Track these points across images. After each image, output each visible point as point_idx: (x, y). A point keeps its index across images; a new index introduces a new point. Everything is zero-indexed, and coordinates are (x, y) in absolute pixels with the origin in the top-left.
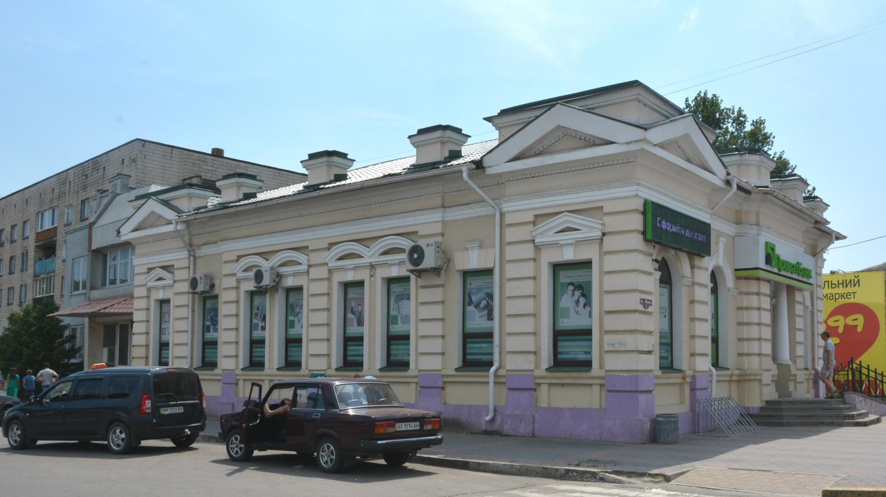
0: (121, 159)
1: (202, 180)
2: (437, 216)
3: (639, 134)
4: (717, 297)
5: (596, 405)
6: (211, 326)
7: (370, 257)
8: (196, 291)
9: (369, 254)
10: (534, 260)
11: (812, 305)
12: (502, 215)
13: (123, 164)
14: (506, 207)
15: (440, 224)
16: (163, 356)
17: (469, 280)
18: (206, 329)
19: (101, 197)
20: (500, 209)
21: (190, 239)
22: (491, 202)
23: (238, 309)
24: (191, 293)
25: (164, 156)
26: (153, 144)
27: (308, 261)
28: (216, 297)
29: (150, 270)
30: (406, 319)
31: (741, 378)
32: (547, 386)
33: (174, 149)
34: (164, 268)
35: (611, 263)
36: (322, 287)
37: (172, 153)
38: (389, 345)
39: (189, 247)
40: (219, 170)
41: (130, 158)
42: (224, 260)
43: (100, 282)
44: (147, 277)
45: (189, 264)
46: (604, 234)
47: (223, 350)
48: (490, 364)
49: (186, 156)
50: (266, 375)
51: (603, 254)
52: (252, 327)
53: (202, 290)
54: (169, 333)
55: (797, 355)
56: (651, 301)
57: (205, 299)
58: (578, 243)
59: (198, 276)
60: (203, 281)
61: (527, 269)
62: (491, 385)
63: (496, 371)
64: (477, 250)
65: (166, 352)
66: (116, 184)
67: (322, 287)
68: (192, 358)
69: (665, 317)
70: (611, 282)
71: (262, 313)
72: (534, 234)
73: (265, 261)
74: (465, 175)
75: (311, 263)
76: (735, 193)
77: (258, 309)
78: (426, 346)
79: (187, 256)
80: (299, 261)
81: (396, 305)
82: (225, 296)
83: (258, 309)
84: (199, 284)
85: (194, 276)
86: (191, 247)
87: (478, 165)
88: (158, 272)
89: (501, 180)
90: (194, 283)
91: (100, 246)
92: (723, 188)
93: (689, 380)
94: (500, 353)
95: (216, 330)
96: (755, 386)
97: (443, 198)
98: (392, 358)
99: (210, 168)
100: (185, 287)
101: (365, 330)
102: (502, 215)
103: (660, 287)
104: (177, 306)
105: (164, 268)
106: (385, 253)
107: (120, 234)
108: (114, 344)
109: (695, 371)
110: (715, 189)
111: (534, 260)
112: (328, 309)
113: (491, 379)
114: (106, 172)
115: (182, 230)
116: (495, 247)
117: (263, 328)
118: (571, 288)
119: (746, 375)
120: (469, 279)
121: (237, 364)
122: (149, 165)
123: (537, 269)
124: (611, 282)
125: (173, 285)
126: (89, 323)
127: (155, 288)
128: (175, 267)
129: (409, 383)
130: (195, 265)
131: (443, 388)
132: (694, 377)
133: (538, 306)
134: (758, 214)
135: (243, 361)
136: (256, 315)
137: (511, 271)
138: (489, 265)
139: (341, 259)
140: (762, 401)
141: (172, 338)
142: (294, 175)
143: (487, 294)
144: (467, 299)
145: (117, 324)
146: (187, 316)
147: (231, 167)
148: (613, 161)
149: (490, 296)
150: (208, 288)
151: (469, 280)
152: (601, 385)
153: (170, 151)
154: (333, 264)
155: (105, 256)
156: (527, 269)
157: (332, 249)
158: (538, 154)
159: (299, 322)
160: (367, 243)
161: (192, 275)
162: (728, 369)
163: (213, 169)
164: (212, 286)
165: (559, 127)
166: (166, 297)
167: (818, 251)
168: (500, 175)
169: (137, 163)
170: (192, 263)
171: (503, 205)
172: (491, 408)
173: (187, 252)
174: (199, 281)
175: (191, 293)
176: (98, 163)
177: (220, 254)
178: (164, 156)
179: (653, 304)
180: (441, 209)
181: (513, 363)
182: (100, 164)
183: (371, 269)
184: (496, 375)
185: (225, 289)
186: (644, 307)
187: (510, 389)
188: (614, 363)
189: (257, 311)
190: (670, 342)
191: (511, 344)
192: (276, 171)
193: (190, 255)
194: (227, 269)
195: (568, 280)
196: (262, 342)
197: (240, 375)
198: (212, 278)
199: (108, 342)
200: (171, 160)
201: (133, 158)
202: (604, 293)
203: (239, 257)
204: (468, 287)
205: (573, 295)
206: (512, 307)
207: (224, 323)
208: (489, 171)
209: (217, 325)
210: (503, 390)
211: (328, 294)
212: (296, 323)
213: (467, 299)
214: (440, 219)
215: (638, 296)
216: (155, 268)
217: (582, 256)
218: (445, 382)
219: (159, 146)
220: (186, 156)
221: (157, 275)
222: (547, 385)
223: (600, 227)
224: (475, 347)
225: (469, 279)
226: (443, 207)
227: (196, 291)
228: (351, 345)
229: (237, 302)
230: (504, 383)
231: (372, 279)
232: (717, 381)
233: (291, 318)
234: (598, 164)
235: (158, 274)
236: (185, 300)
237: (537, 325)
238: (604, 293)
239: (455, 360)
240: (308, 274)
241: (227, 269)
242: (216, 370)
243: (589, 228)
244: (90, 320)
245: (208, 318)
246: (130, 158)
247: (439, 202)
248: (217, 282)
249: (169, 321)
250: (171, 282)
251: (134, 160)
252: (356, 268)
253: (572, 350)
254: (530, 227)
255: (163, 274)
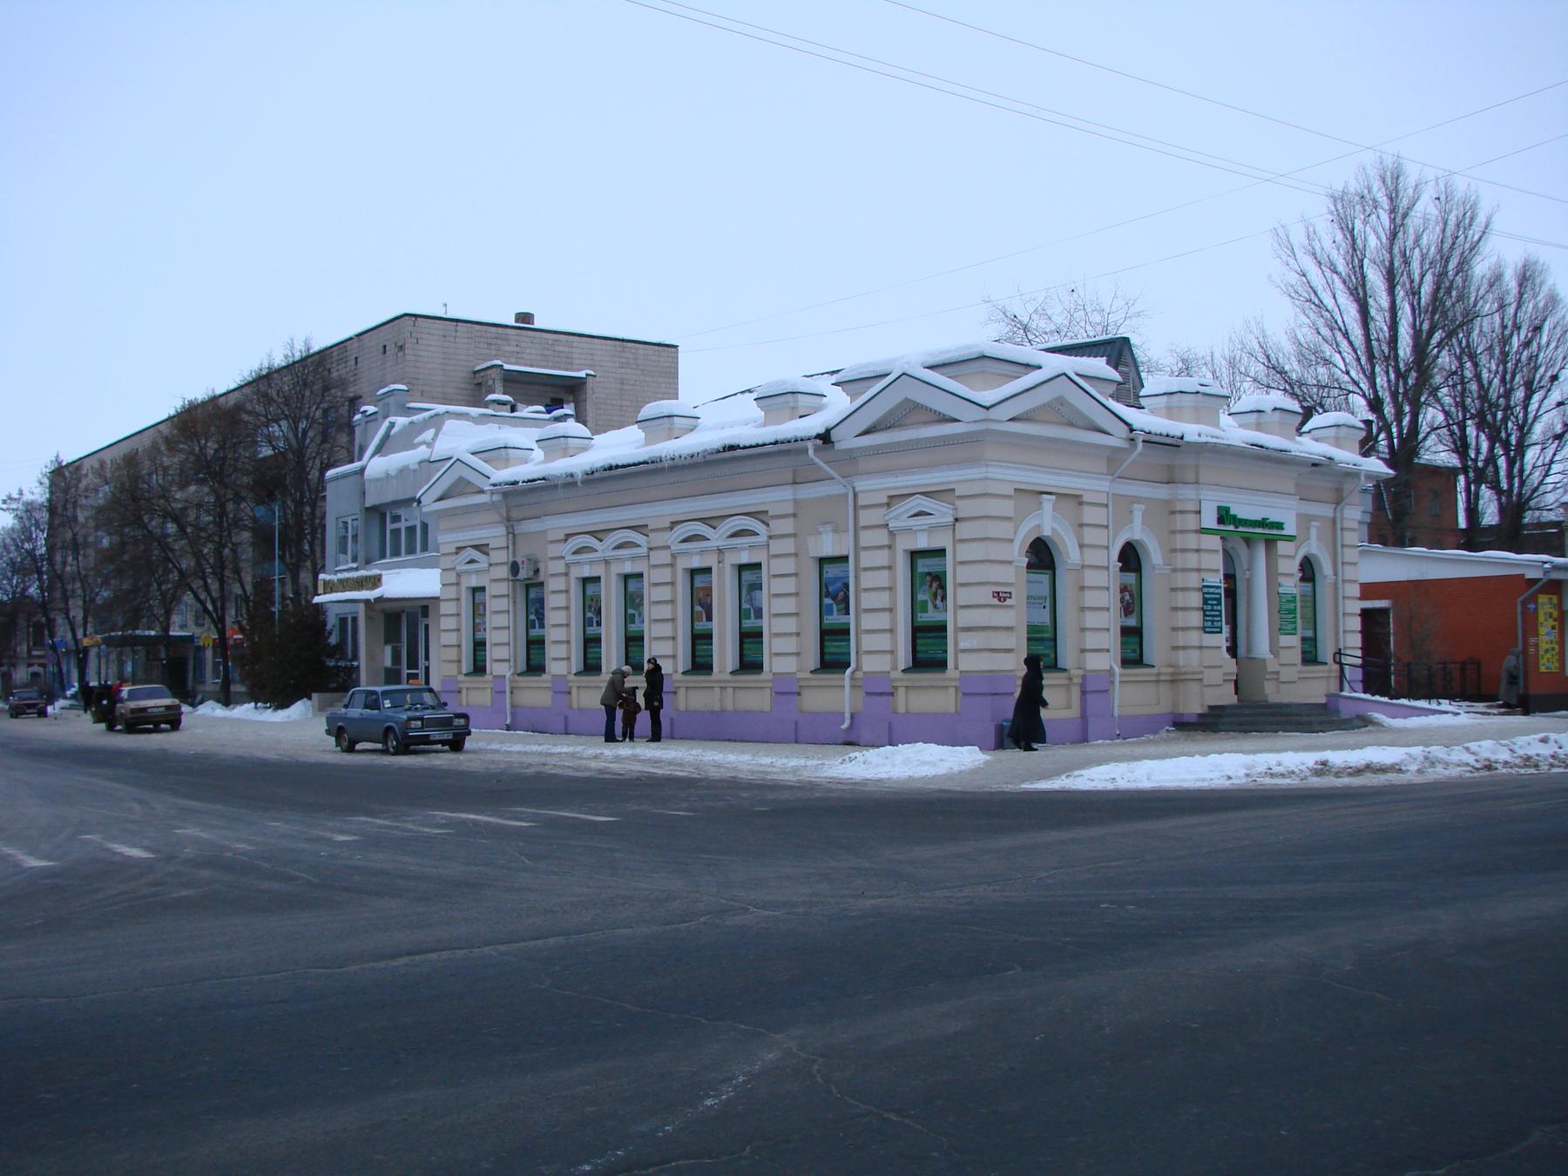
0: (381, 346)
1: (503, 372)
2: (787, 493)
3: (982, 414)
4: (1141, 577)
5: (952, 709)
6: (537, 622)
7: (717, 539)
8: (518, 578)
9: (716, 537)
10: (889, 547)
11: (1336, 574)
12: (855, 495)
13: (385, 352)
14: (861, 484)
15: (792, 503)
16: (478, 658)
17: (826, 567)
18: (530, 625)
19: (367, 422)
20: (854, 488)
21: (508, 511)
22: (842, 480)
23: (568, 600)
24: (512, 580)
25: (444, 336)
26: (429, 320)
27: (648, 543)
28: (542, 584)
29: (459, 549)
30: (759, 613)
31: (1175, 678)
32: (719, 689)
33: (460, 324)
34: (475, 547)
35: (965, 552)
36: (665, 575)
37: (456, 331)
38: (741, 643)
39: (506, 522)
40: (528, 351)
41: (396, 344)
42: (550, 538)
43: (376, 551)
44: (456, 559)
45: (508, 543)
46: (956, 520)
47: (552, 651)
48: (848, 665)
49: (479, 334)
50: (717, 682)
51: (956, 541)
52: (587, 622)
53: (525, 577)
54: (485, 630)
55: (1281, 645)
56: (1010, 593)
57: (528, 587)
58: (933, 529)
59: (519, 560)
60: (525, 566)
61: (882, 558)
62: (847, 689)
63: (853, 672)
64: (831, 534)
65: (483, 653)
66: (388, 404)
67: (665, 575)
68: (515, 661)
69: (1044, 607)
70: (965, 574)
71: (597, 605)
72: (887, 518)
73: (598, 541)
74: (811, 452)
75: (652, 546)
76: (1140, 454)
77: (592, 600)
78: (780, 645)
79: (505, 533)
80: (638, 543)
81: (749, 597)
82: (553, 584)
83: (592, 600)
84: (521, 570)
85: (515, 559)
86: (510, 523)
87: (825, 437)
88: (469, 552)
89: (852, 456)
90: (515, 568)
91: (377, 503)
92: (1125, 449)
93: (1077, 680)
94: (857, 652)
95: (542, 626)
96: (1194, 688)
97: (794, 472)
98: (746, 659)
99: (515, 349)
100: (504, 572)
101: (715, 626)
102: (855, 495)
103: (1027, 572)
104: (495, 597)
105: (475, 547)
106: (734, 535)
107: (421, 505)
108: (399, 640)
109: (1085, 670)
110: (1116, 450)
111: (889, 547)
112: (673, 602)
113: (847, 682)
114: (359, 365)
115: (497, 501)
116: (848, 531)
117: (599, 624)
118: (928, 578)
119: (1180, 674)
120: (825, 566)
121: (675, 665)
122: (423, 353)
123: (893, 558)
124: (965, 574)
125: (489, 570)
126: (366, 612)
127: (467, 572)
128: (491, 546)
129: (763, 688)
130: (514, 544)
131: (799, 694)
132: (1084, 677)
133: (894, 599)
134: (1197, 467)
135: (576, 663)
136: (590, 607)
137: (867, 559)
138: (844, 553)
139: (684, 541)
140: (1202, 705)
141: (491, 637)
142: (647, 346)
143: (844, 583)
144: (824, 590)
145: (403, 611)
146: (507, 609)
147: (546, 344)
148: (953, 441)
149: (846, 586)
150: (531, 574)
151: (826, 567)
152: (771, 688)
153: (453, 328)
154: (676, 547)
155: (383, 516)
156: (882, 558)
157: (675, 529)
158: (890, 427)
159: (640, 616)
160: (714, 523)
161: (511, 559)
162: (1326, 664)
163: (518, 349)
164: (537, 571)
165: (907, 400)
166: (481, 584)
167: (1345, 496)
168: (851, 450)
169: (406, 352)
170: (511, 542)
171: (856, 484)
172: (847, 715)
173: (505, 529)
174: (521, 566)
175: (512, 580)
176: (346, 351)
177: (545, 532)
178: (444, 336)
179: (1013, 596)
180: (789, 486)
181: (871, 664)
182: (349, 353)
183: (719, 553)
184: (852, 678)
185: (552, 575)
186: (1000, 600)
187: (868, 694)
188: (969, 663)
189: (590, 603)
190: (1053, 637)
191: (868, 642)
192: (618, 343)
193: (508, 533)
194: (554, 550)
195: (926, 570)
196: (598, 640)
197: (574, 681)
198: (536, 562)
199: (392, 636)
200: (455, 343)
201: (399, 344)
202: (957, 585)
203: (568, 536)
204: (825, 575)
205: (931, 586)
206: (868, 600)
207: (552, 617)
208: (837, 446)
209: (544, 619)
210: (861, 695)
211: (672, 584)
212: (637, 616)
213: (824, 590)
214: (791, 497)
215: (989, 590)
216: (465, 547)
217: (936, 544)
218: (800, 686)
219: (438, 321)
220: (479, 334)
221: (467, 557)
222: (904, 689)
223: (951, 512)
224: (833, 647)
225: (825, 566)
226: (795, 483)
227: (518, 578)
228: (699, 644)
229: (567, 591)
230: (860, 687)
231: (721, 565)
232: (1121, 682)
233: (631, 611)
234: (953, 441)
235: (470, 554)
236: (503, 588)
237: (894, 621)
238: (957, 585)
239: (813, 660)
240: (649, 559)
241: (554, 550)
242: (544, 675)
243: (942, 512)
244: (366, 607)
245: (533, 610)
246: (396, 344)
247: (790, 478)
248: (542, 566)
249: (485, 615)
250: (485, 565)
251: (401, 346)
252: (702, 552)
253: (928, 647)
254: (883, 510)
255: (476, 555)
